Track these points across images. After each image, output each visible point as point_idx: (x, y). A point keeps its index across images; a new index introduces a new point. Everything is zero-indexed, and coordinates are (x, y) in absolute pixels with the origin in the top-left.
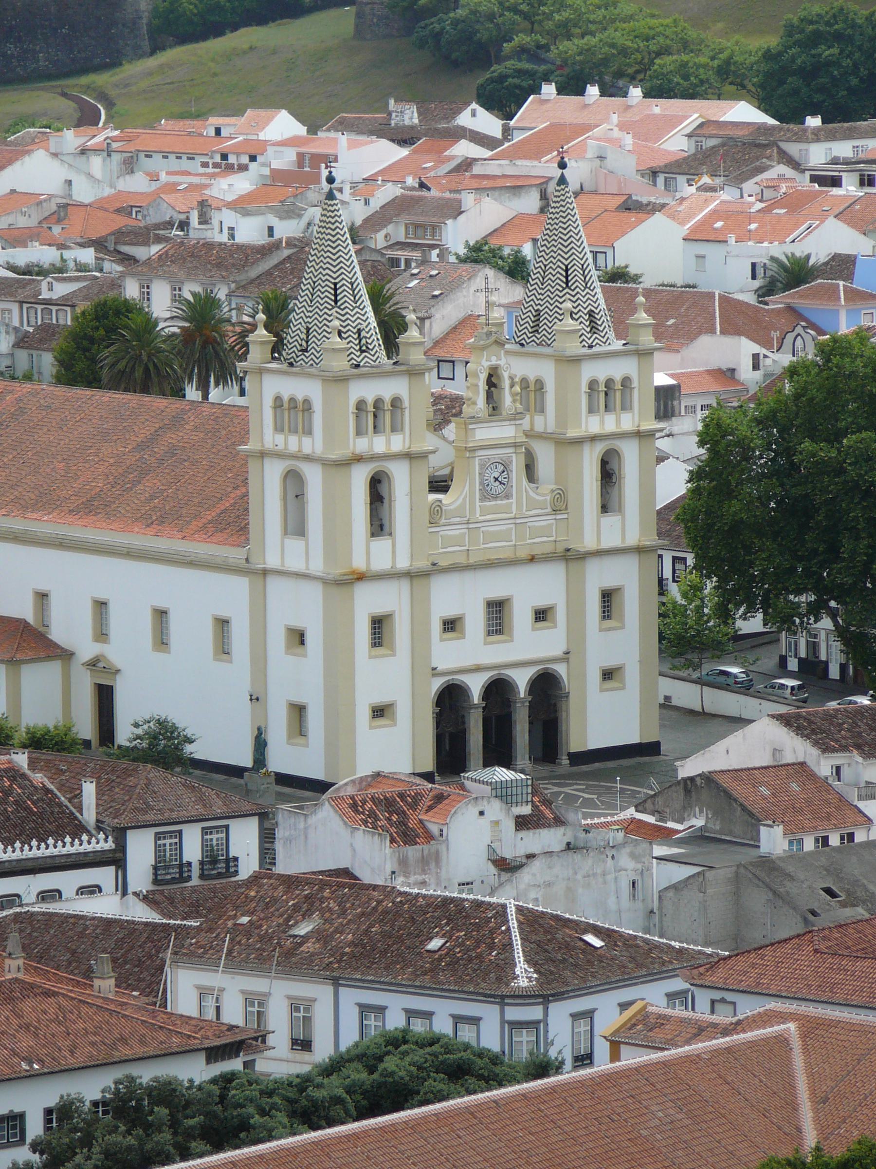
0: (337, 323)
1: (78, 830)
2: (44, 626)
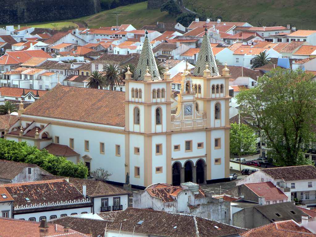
0: (148, 69)
1: (81, 197)
2: (72, 147)
